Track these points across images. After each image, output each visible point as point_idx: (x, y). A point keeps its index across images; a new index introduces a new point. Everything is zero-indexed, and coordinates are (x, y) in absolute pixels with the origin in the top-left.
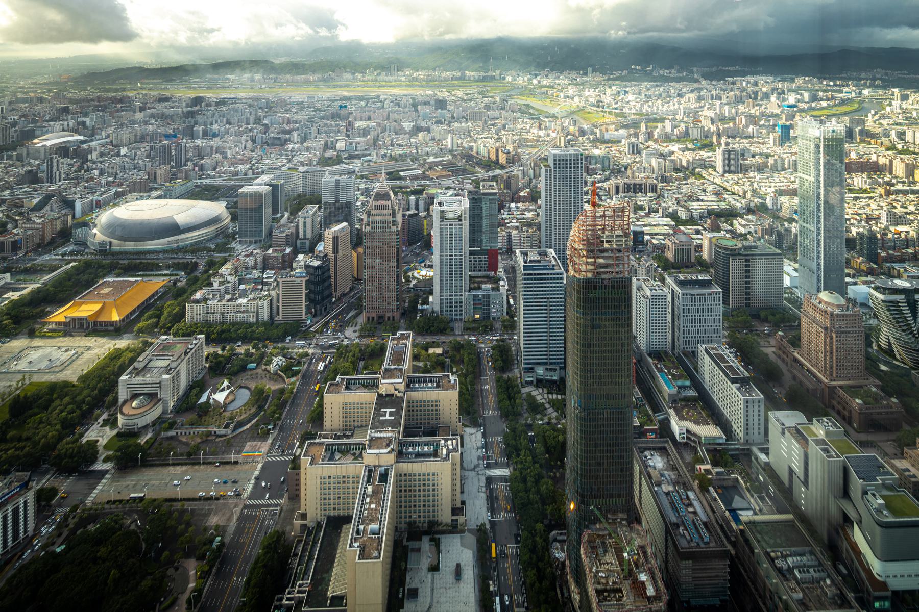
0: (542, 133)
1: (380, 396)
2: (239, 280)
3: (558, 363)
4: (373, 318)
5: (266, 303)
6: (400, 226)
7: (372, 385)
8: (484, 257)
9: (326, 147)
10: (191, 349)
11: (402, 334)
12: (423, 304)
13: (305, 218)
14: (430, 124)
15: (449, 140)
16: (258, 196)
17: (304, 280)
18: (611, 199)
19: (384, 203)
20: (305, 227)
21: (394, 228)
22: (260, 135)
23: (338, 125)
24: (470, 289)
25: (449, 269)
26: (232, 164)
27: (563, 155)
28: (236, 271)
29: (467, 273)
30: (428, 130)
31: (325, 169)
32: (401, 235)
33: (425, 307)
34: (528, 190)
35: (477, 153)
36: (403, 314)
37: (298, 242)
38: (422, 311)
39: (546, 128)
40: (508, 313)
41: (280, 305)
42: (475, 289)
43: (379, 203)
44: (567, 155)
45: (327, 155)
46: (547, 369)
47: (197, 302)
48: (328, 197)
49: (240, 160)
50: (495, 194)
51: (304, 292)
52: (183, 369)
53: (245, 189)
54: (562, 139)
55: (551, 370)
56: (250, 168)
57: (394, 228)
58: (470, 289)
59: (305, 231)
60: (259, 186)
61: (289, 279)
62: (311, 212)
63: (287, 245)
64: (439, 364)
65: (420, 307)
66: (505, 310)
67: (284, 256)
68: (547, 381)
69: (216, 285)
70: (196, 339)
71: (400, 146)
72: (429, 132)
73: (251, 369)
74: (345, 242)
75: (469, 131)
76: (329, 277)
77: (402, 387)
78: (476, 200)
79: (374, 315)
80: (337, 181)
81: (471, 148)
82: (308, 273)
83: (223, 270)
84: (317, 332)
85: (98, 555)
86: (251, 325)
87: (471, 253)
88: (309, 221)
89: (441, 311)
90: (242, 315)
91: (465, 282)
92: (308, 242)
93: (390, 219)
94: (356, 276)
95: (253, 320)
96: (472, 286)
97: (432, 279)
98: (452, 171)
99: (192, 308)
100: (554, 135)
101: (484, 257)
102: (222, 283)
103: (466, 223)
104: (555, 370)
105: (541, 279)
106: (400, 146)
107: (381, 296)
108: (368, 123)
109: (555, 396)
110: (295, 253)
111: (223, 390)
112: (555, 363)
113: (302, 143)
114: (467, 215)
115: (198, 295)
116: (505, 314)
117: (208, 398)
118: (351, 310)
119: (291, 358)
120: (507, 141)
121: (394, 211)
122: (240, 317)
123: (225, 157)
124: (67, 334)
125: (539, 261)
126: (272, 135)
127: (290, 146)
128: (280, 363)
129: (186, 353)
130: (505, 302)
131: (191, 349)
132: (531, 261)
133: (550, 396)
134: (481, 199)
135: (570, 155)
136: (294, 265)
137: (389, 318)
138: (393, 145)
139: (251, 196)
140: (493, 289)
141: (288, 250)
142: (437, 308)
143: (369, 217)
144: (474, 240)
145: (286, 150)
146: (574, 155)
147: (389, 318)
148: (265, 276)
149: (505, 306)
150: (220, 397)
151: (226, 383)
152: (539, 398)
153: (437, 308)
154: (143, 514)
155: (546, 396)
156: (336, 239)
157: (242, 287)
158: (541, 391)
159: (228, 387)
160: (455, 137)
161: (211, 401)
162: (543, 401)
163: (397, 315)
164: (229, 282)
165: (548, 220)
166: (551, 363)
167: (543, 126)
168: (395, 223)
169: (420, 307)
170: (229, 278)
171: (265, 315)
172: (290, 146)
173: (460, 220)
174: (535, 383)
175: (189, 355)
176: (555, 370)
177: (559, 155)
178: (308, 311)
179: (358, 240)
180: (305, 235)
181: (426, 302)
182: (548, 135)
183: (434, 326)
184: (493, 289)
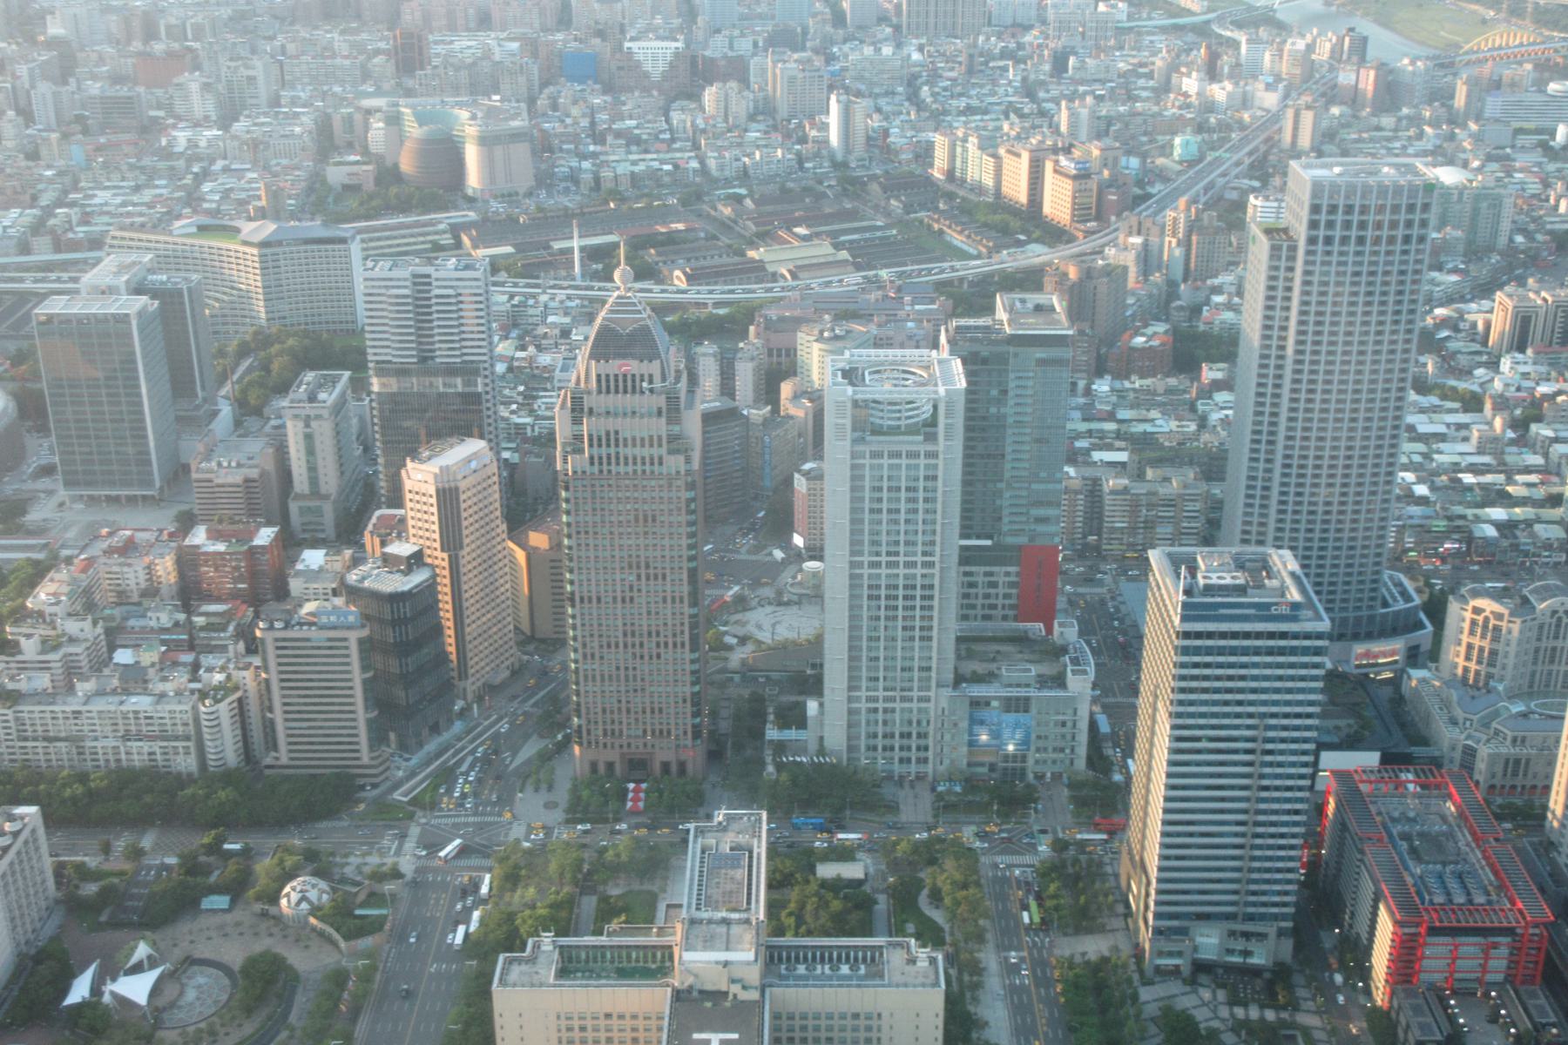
0: (1220, 92)
1: (678, 996)
2: (109, 632)
3: (1275, 917)
4: (610, 765)
5: (224, 709)
7: (653, 965)
9: (327, 141)
11: (729, 818)
12: (784, 724)
13: (307, 421)
14: (744, 46)
15: (834, 119)
16: (101, 336)
17: (353, 637)
18: (1494, 365)
19: (633, 366)
20: (310, 451)
22: (44, 88)
23: (359, 48)
24: (959, 680)
25: (887, 604)
27: (1351, 190)
29: (947, 625)
30: (737, 70)
31: (346, 229)
33: (792, 734)
34: (1161, 328)
35: (950, 174)
37: (294, 507)
38: (780, 747)
39: (1237, 73)
41: (278, 716)
42: (977, 679)
43: (615, 367)
44: (1367, 190)
45: (336, 175)
46: (1232, 934)
48: (386, 342)
50: (1060, 341)
53: (56, 306)
54: (1307, 118)
55: (1247, 935)
56: (37, 228)
57: (675, 463)
58: (959, 680)
59: (312, 469)
61: (295, 633)
62: (328, 397)
64: (852, 910)
65: (772, 733)
66: (1082, 751)
67: (253, 551)
68: (1230, 968)
72: (744, 82)
75: (912, 82)
76: (438, 630)
77: (754, 975)
79: (613, 756)
80: (421, 283)
81: (924, 154)
82: (366, 617)
84: (415, 802)
86: (182, 781)
87: (968, 557)
88: (324, 431)
90: (146, 746)
91: (942, 650)
93: (660, 427)
94: (525, 626)
95: (186, 763)
96: (971, 667)
97: (817, 643)
98: (851, 246)
100: (1270, 100)
102: (48, 645)
103: (950, 450)
104: (1262, 936)
105: (1245, 651)
106: (632, 140)
108: (490, 39)
109: (1254, 1013)
110: (290, 543)
111: (137, 969)
112: (1263, 917)
114: (959, 421)
117: (96, 990)
118: (526, 737)
121: (672, 400)
122: (138, 753)
125: (1241, 590)
126: (94, 88)
127: (181, 137)
128: (313, 895)
132: (1209, 589)
133: (1240, 1012)
134: (1003, 359)
135: (1383, 190)
136: (295, 585)
138: (599, 139)
139: (80, 322)
141: (265, 536)
142: (836, 738)
144: (977, 514)
146: (1398, 190)
147: (666, 767)
148: (199, 620)
150: (136, 988)
151: (142, 950)
152: (1201, 1015)
153: (836, 738)
155: (1224, 1012)
156: (448, 498)
157: (123, 656)
158: (1206, 995)
159: (152, 963)
160: (862, 105)
161: (107, 998)
162: (1215, 1024)
164: (72, 640)
165: (1264, 438)
166: (1251, 918)
167: (1226, 62)
168: (676, 443)
170: (72, 627)
171: (225, 748)
173: (931, 438)
174: (1186, 970)
176: (1262, 936)
177: (1334, 188)
179: (524, 500)
180: (314, 481)
182: (1245, 102)
183: (827, 794)
184: (1043, 682)
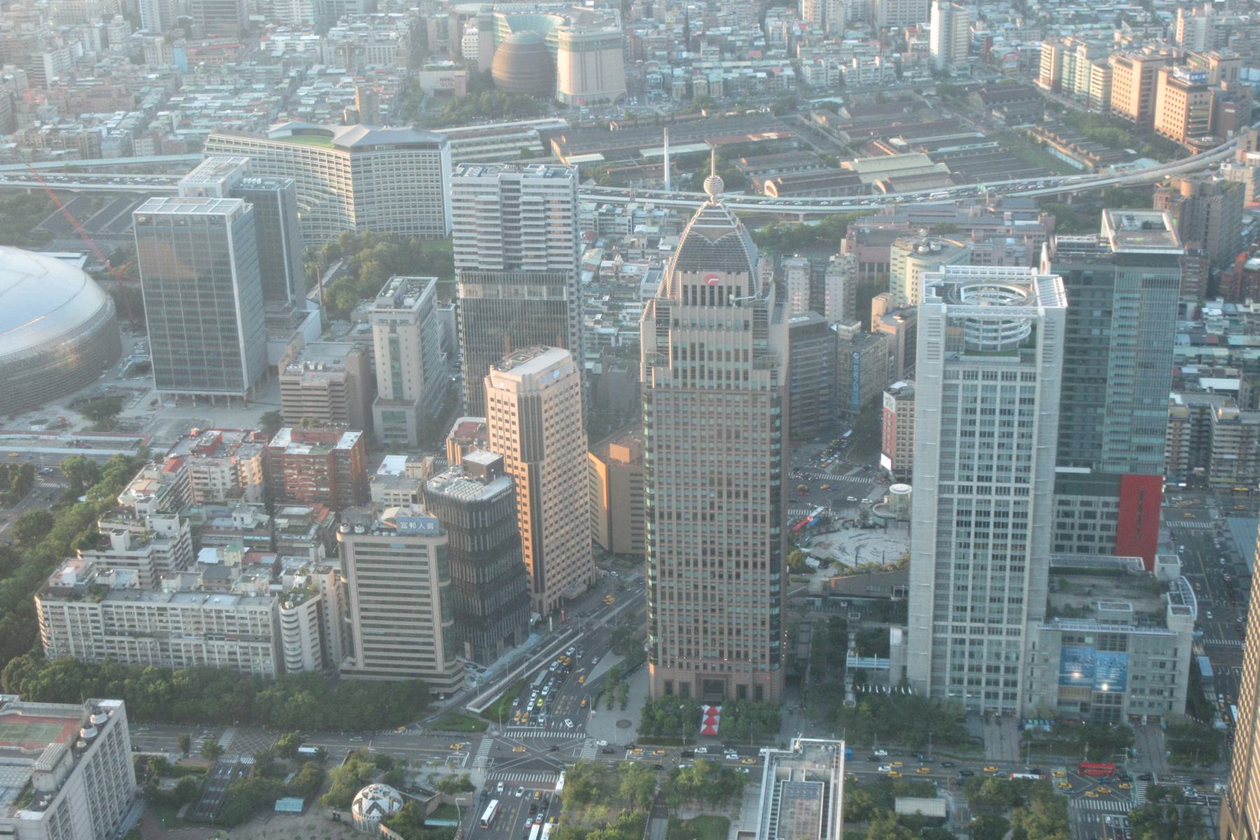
2: (195, 531)
4: (685, 687)
8: (1104, 503)
10: (90, 742)
12: (865, 652)
13: (393, 326)
17: (432, 544)
19: (720, 278)
20: (395, 357)
21: (761, 378)
26: (70, 109)
28: (174, 502)
32: (785, 401)
33: (873, 662)
35: (1056, 85)
36: (793, 681)
37: (377, 412)
38: (861, 676)
40: (1190, 705)
42: (1071, 613)
43: (701, 278)
45: (429, 80)
47: (73, 594)
48: (472, 248)
49: (96, 94)
51: (435, 585)
52: (76, 792)
53: (155, 207)
57: (761, 378)
58: (1051, 613)
59: (396, 374)
60: (200, 193)
62: (414, 303)
63: (337, 417)
65: (853, 661)
66: (1182, 694)
67: (336, 456)
69: (119, 543)
70: (97, 711)
71: (726, 48)
74: (566, 416)
76: (516, 540)
78: (1087, 281)
79: (689, 676)
80: (510, 188)
81: (1030, 63)
83: (132, 494)
86: (261, 682)
87: (1063, 485)
89: (935, 680)
90: (227, 646)
92: (411, 415)
93: (747, 341)
94: (604, 542)
95: (264, 664)
96: (1062, 600)
99: (57, 614)
101: (1104, 503)
102: (138, 542)
107: (714, 615)
110: (373, 448)
113: (322, 28)
115: (68, 573)
116: (1180, 708)
119: (415, 789)
120: (1190, 34)
121: (760, 313)
122: (220, 653)
123: (36, 77)
124: (779, 501)
129: (79, 753)
130: (1184, 667)
131: (90, 742)
134: (1107, 279)
136: (376, 491)
137: (742, 690)
138: (692, 45)
140: (1141, 619)
141: (348, 440)
144: (1072, 441)
145: (266, 58)
147: (742, 690)
148: (282, 522)
149: (1183, 681)
153: (919, 669)
156: (530, 407)
164: (160, 537)
168: (763, 358)
169: (853, 661)
170: (161, 524)
172: (280, 41)
173: (1029, 359)
175: (88, 757)
178: (453, 648)
179: (606, 412)
180: (397, 386)
184: (1141, 619)
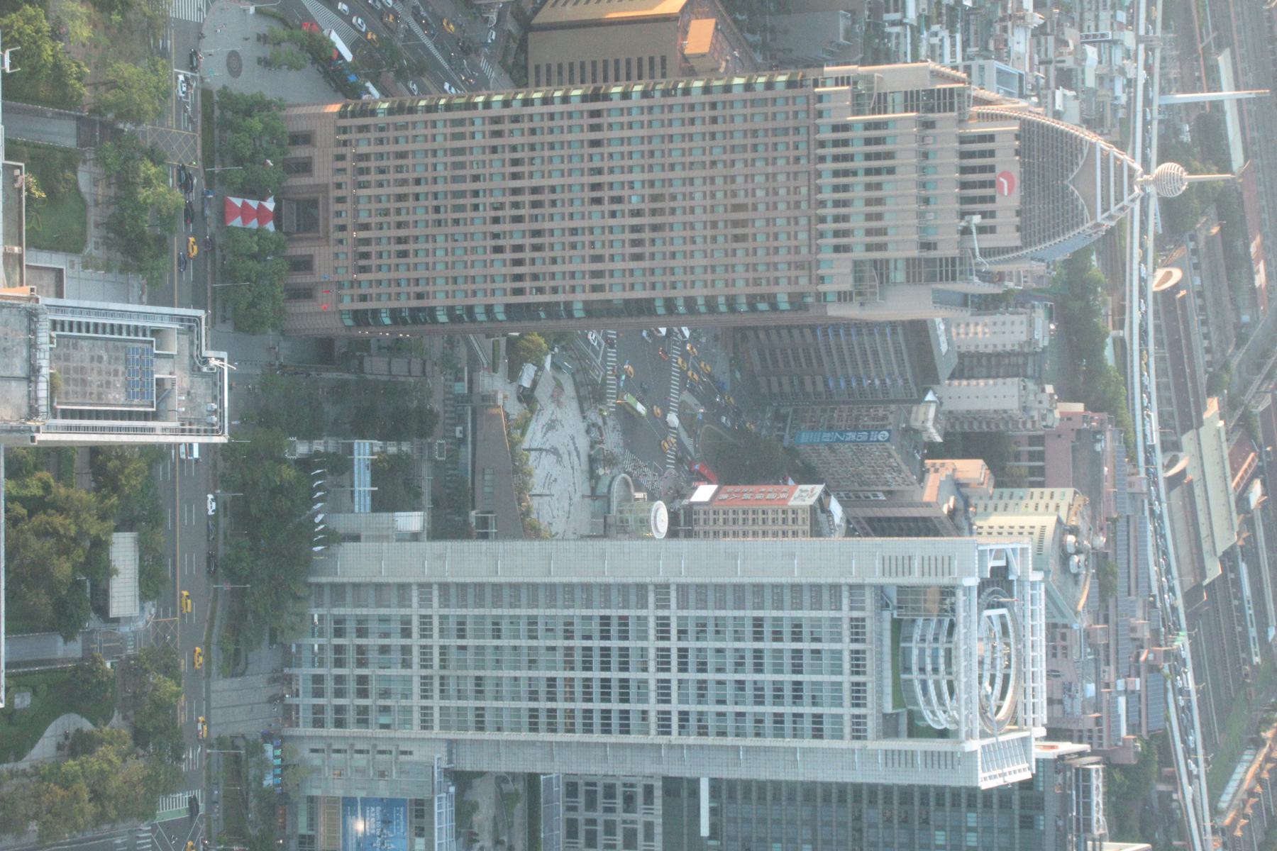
4: (305, 167)
6: (851, 312)
19: (1008, 198)
33: (363, 484)
36: (325, 350)
38: (340, 465)
43: (1007, 164)
57: (839, 274)
58: (462, 780)
65: (364, 451)
73: (535, 383)
79: (323, 172)
85: (127, 127)
87: (679, 791)
89: (338, 591)
93: (902, 249)
96: (484, 797)
121: (949, 269)
137: (304, 264)
143: (911, 100)
147: (304, 264)
154: (388, 462)
163: (325, 314)
168: (872, 277)
173: (889, 727)
181: (393, 490)
